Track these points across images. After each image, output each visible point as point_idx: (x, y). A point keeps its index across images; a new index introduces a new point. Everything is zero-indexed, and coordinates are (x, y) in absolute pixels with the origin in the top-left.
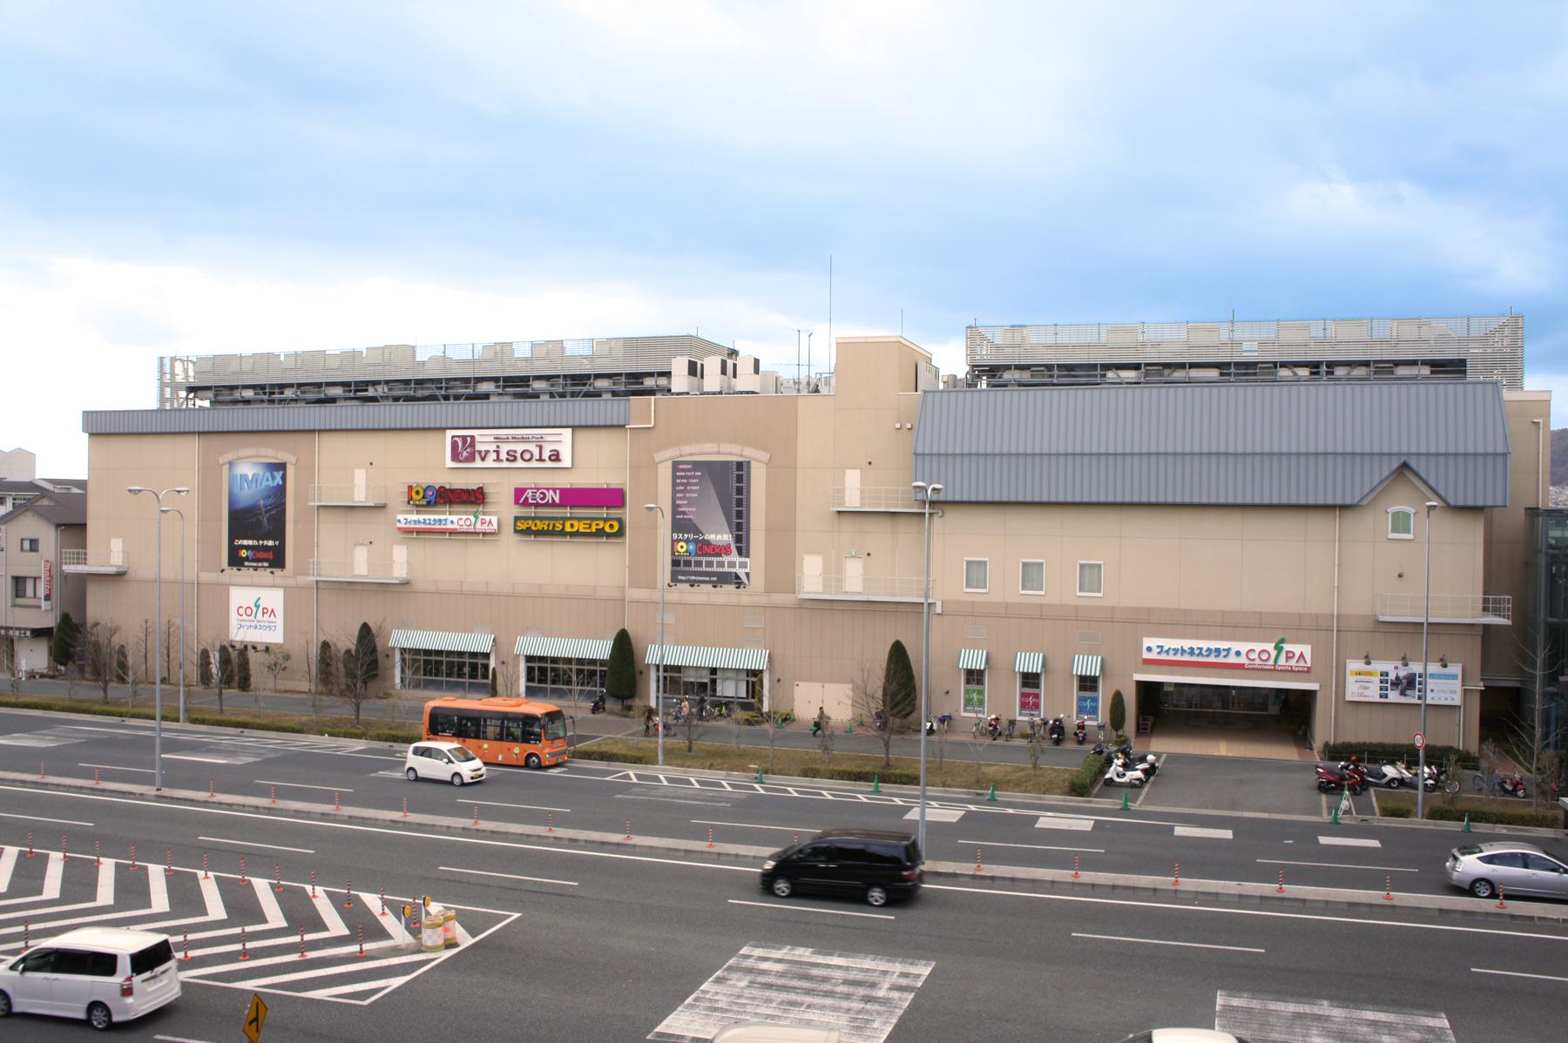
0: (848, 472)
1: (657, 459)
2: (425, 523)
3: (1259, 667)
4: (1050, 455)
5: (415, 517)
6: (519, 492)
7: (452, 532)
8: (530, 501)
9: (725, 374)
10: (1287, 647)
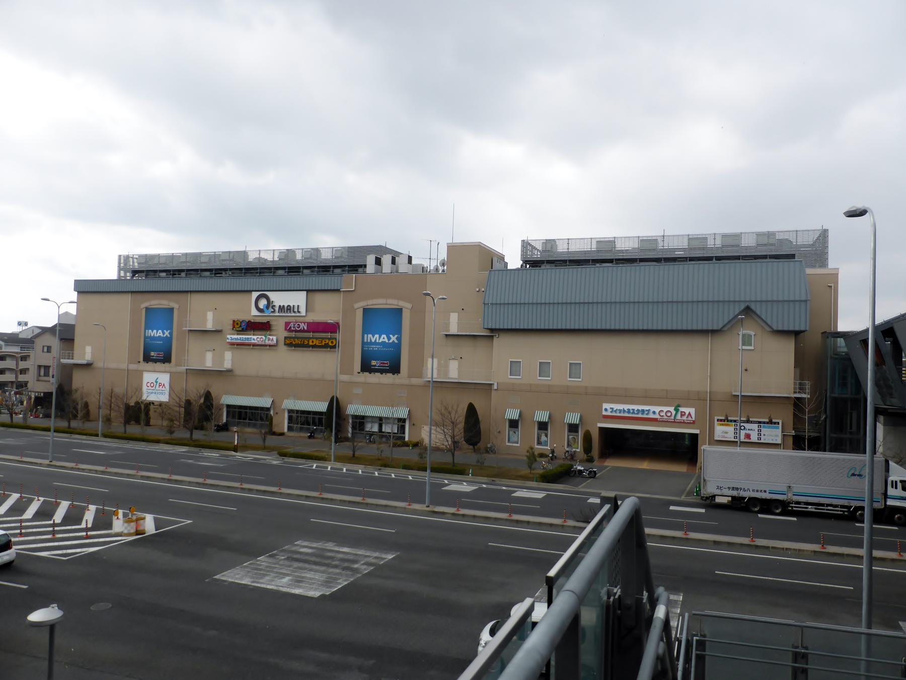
0: (452, 314)
2: (240, 340)
3: (666, 420)
4: (616, 303)
5: (236, 337)
6: (287, 324)
7: (254, 345)
8: (292, 329)
9: (394, 264)
10: (682, 409)
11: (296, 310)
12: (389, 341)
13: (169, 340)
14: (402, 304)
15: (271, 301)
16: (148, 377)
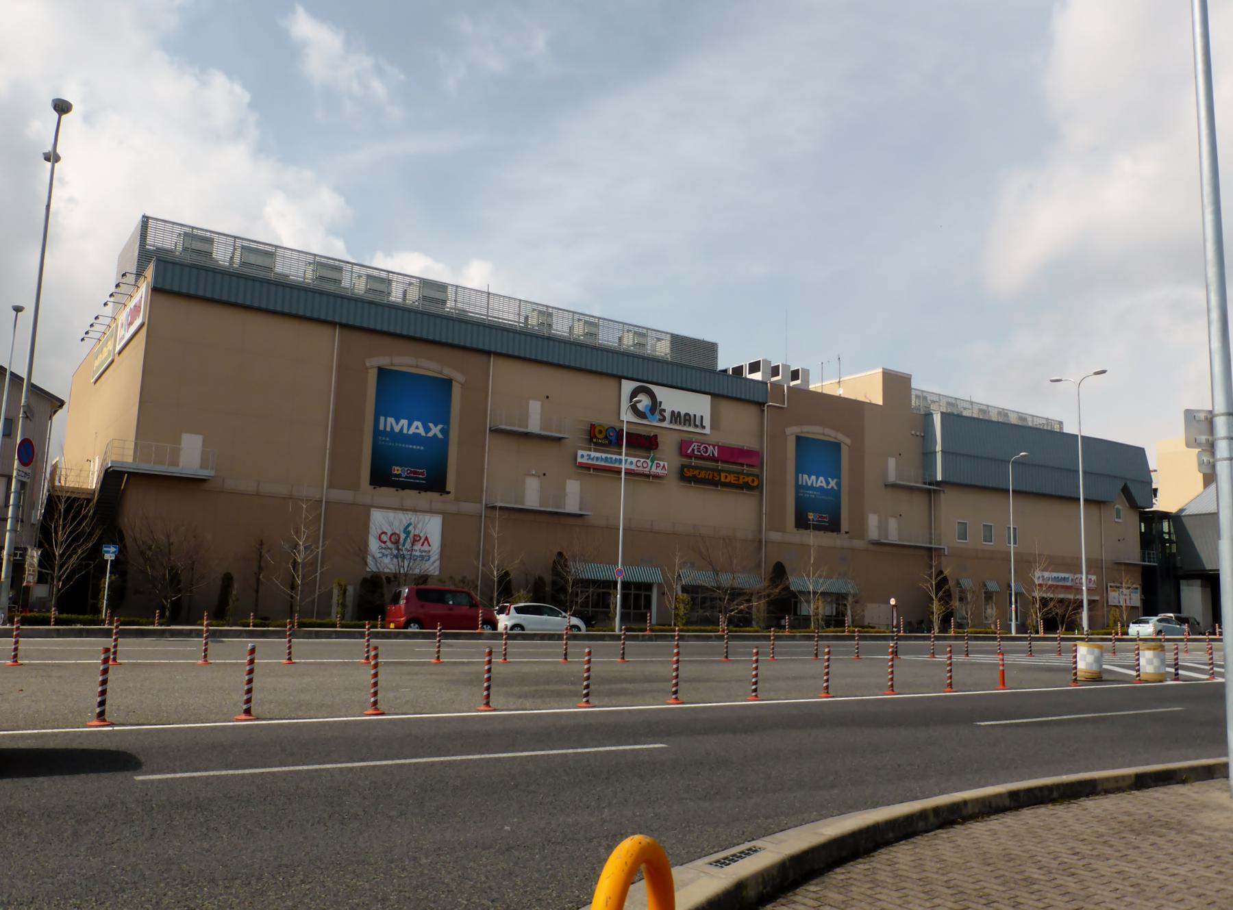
1: (368, 364)
5: (593, 454)
11: (698, 423)
12: (426, 434)
13: (440, 446)
14: (841, 437)
15: (658, 400)
16: (383, 521)
